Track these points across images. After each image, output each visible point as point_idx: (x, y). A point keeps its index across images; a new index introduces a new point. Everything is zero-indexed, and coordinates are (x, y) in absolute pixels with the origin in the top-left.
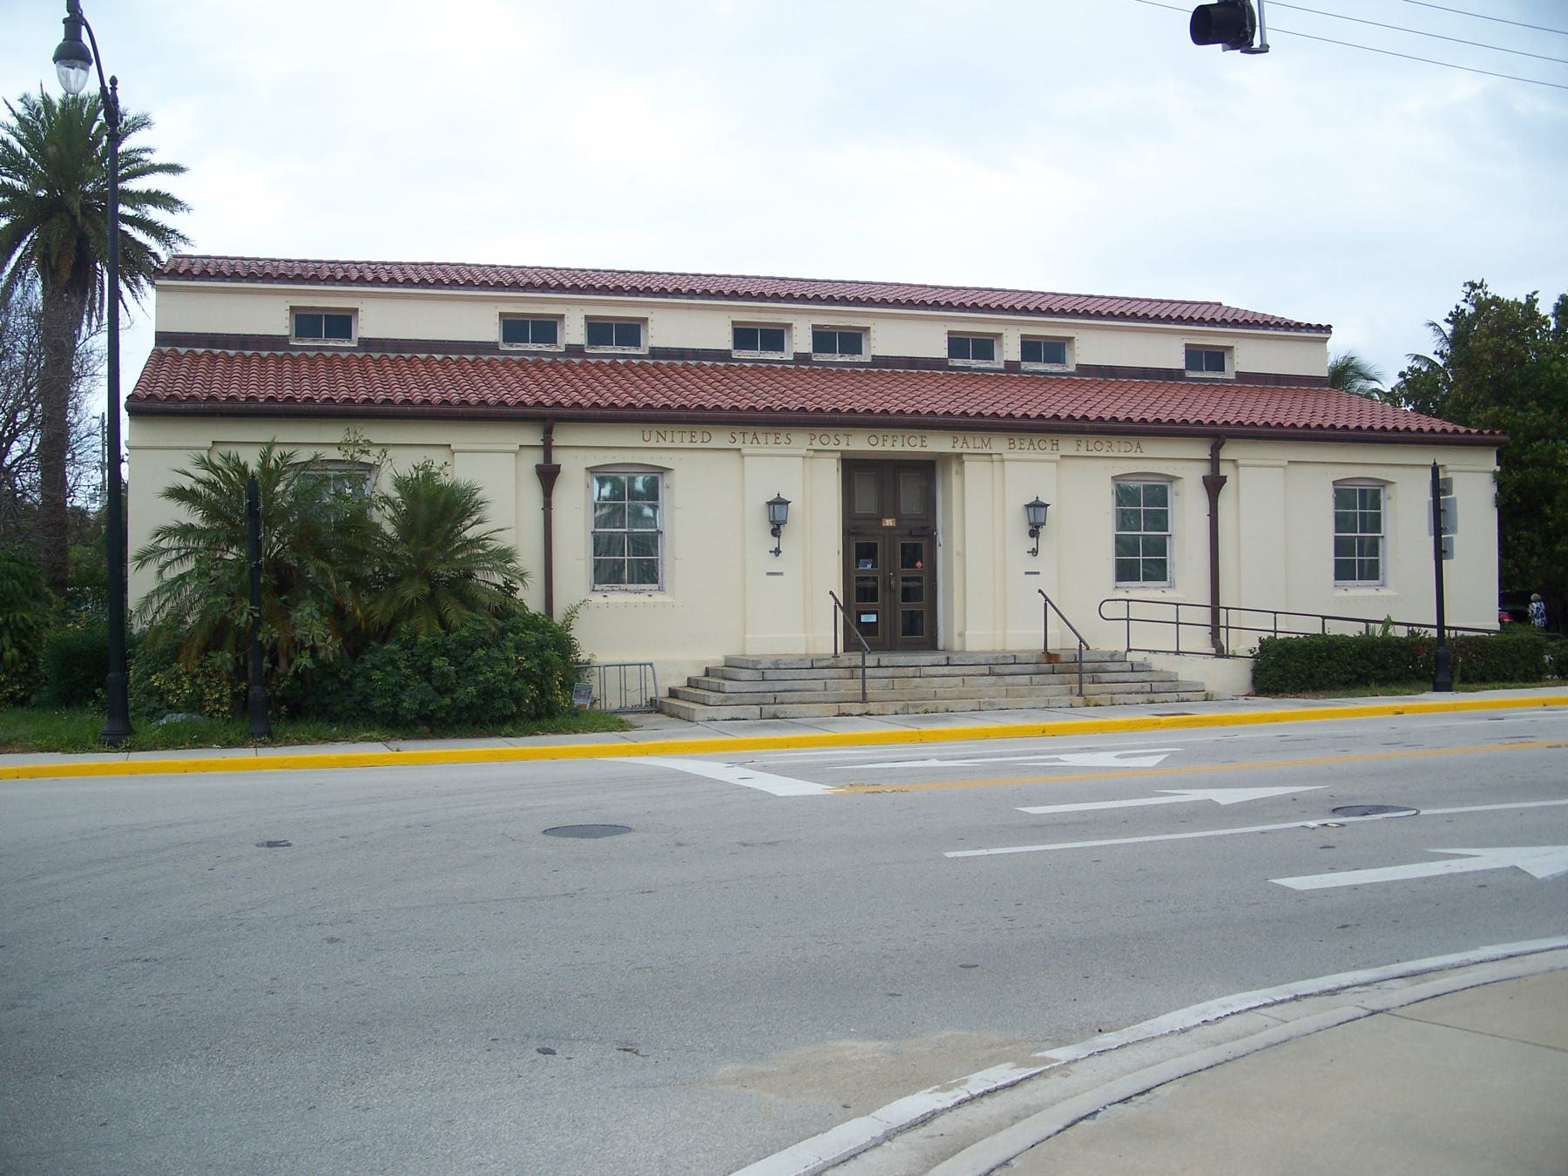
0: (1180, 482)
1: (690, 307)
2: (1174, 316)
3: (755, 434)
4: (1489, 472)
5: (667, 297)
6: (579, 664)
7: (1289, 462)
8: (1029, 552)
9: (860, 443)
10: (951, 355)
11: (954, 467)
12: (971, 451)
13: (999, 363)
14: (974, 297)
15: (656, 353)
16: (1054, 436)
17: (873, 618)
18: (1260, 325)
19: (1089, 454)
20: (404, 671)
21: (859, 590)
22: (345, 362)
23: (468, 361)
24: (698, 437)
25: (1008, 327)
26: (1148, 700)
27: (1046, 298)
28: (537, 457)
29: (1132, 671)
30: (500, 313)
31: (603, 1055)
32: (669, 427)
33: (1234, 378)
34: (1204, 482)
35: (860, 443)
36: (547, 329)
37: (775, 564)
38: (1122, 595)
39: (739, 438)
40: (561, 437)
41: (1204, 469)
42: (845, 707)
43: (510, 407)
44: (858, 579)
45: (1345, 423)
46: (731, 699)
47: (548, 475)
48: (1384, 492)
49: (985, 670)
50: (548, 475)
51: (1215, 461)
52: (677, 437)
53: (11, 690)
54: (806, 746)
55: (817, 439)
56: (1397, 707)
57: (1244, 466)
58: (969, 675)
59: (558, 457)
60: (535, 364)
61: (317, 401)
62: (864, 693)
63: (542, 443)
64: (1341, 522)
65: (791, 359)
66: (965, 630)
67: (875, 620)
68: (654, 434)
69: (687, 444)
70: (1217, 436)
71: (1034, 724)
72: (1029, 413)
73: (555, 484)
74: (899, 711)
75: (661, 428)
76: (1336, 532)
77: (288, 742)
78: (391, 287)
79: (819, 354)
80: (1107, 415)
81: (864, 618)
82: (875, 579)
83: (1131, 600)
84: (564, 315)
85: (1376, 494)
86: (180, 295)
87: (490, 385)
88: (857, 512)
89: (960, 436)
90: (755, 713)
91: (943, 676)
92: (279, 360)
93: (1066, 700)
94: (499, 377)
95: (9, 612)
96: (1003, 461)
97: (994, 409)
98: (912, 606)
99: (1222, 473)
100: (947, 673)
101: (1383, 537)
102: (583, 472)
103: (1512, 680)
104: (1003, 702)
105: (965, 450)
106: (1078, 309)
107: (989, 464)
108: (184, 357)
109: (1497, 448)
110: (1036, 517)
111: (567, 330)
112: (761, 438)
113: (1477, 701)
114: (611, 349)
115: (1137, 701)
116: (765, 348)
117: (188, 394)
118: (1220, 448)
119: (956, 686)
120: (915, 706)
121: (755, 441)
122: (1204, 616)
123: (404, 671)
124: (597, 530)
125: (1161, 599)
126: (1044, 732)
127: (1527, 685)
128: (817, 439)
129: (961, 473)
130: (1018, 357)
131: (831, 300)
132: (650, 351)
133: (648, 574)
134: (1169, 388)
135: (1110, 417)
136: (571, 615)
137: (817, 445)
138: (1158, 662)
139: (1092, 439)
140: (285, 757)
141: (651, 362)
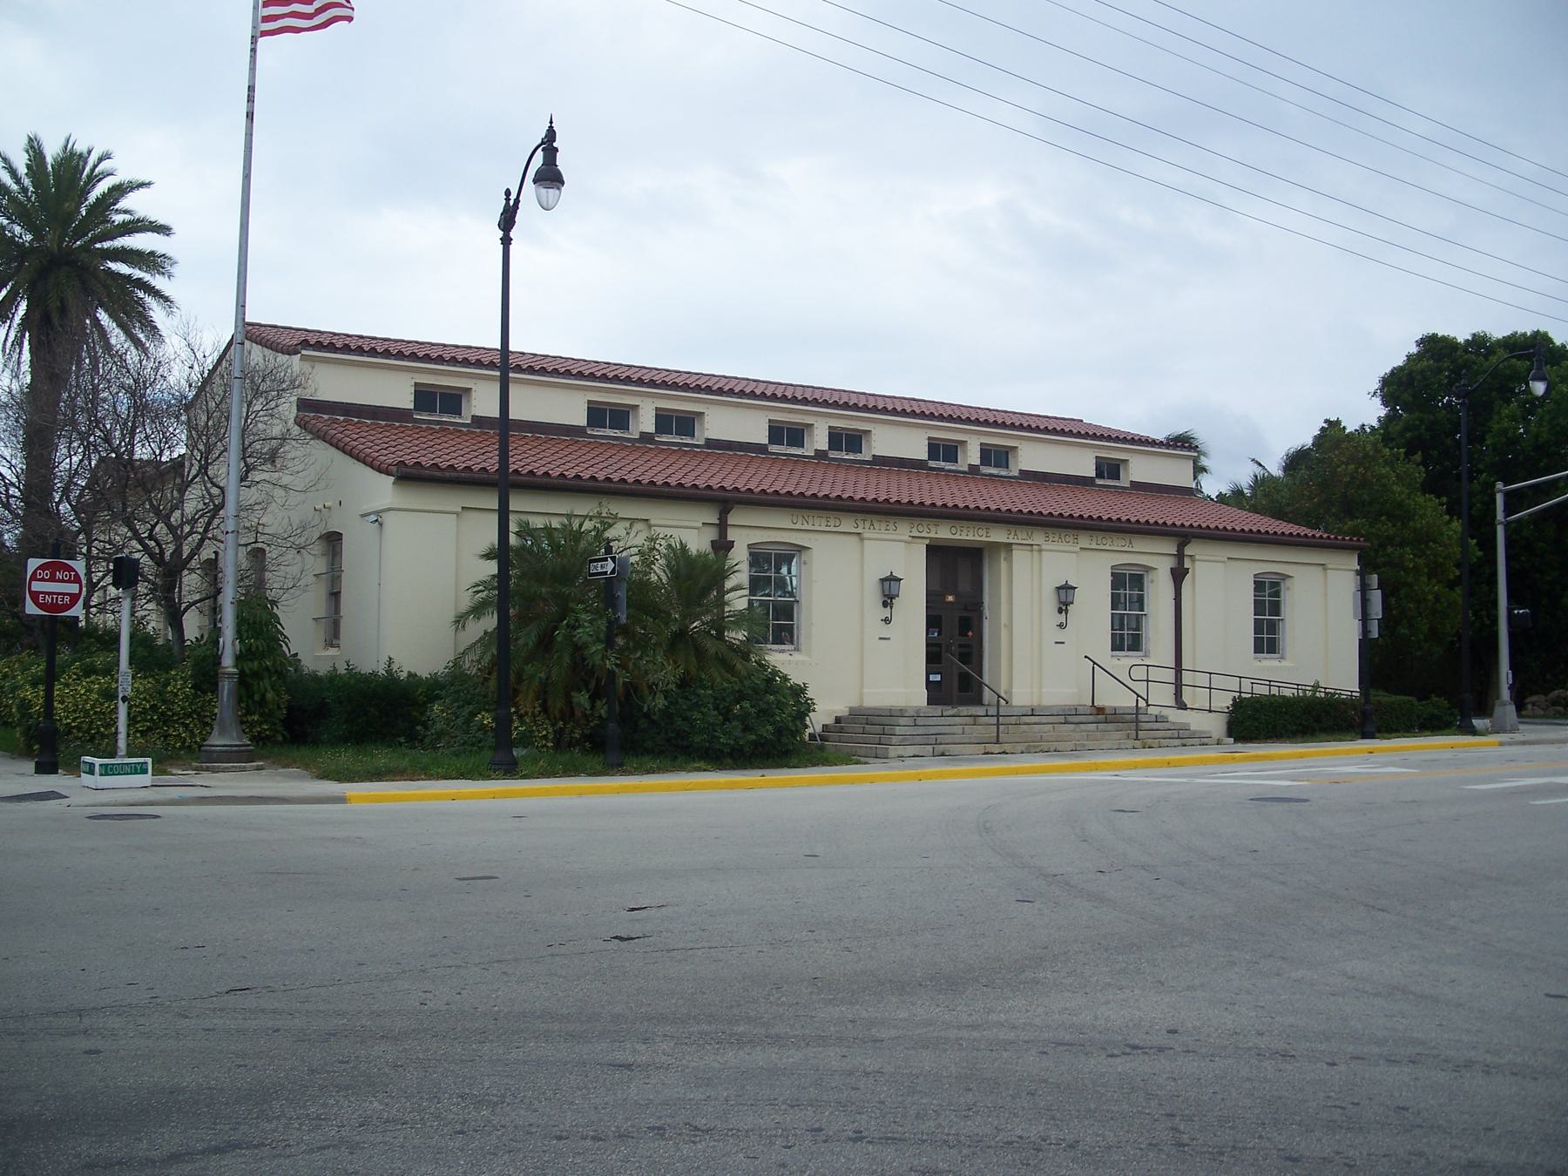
0: (808, 552)
2: (726, 388)
5: (722, 396)
7: (1228, 558)
9: (944, 532)
10: (771, 442)
11: (1003, 555)
12: (1017, 542)
13: (961, 466)
14: (530, 361)
17: (938, 678)
18: (936, 417)
19: (828, 529)
27: (589, 366)
31: (1132, 991)
33: (966, 469)
34: (1172, 574)
35: (944, 532)
37: (885, 631)
39: (860, 524)
45: (875, 496)
46: (907, 740)
48: (1148, 577)
49: (1062, 719)
51: (1180, 556)
52: (817, 521)
53: (259, 729)
54: (1042, 772)
57: (1198, 560)
59: (732, 535)
63: (718, 522)
64: (1116, 602)
66: (1012, 688)
67: (939, 679)
68: (800, 518)
70: (1183, 536)
72: (581, 474)
75: (806, 513)
76: (1255, 615)
80: (616, 477)
85: (1277, 584)
86: (915, 430)
93: (1130, 743)
96: (1040, 551)
99: (730, 538)
100: (1037, 721)
103: (1397, 731)
104: (1090, 744)
105: (1013, 541)
106: (678, 381)
107: (1029, 553)
110: (1065, 596)
113: (1410, 745)
116: (443, 411)
118: (729, 512)
120: (1035, 747)
122: (1170, 675)
127: (1408, 735)
129: (1009, 559)
130: (977, 462)
131: (836, 405)
134: (695, 456)
135: (589, 476)
140: (688, 781)
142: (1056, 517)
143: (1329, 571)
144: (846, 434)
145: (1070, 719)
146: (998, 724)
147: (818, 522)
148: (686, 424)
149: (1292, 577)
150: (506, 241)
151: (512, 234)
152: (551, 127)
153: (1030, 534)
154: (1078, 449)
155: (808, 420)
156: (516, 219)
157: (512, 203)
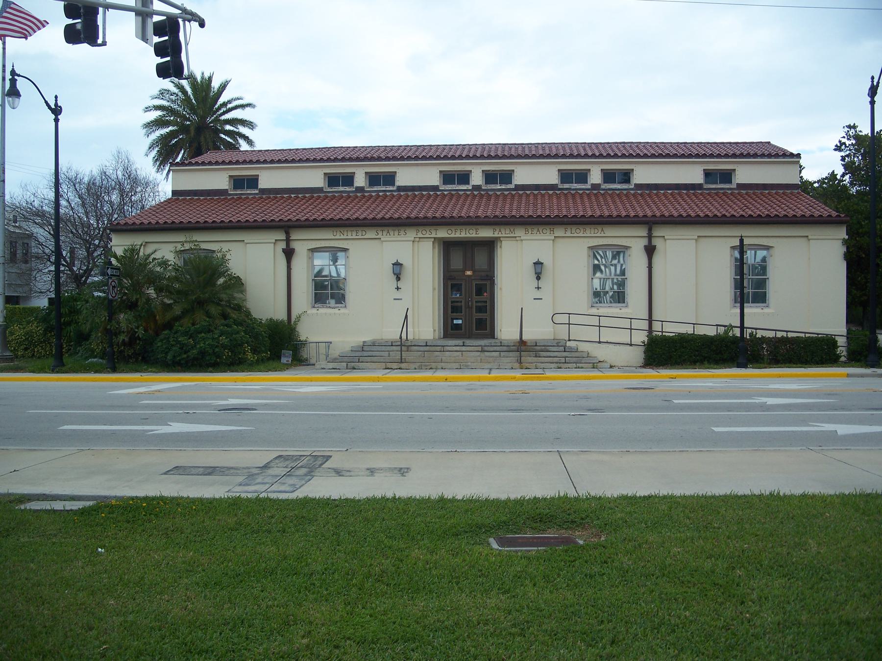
1: (417, 165)
3: (602, 229)
4: (841, 239)
6: (301, 341)
8: (400, 288)
9: (443, 233)
15: (741, 186)
16: (551, 227)
20: (171, 342)
21: (452, 307)
22: (588, 195)
23: (609, 194)
24: (360, 233)
25: (593, 165)
26: (558, 366)
28: (283, 245)
29: (565, 351)
30: (601, 169)
32: (345, 229)
34: (283, 252)
36: (348, 179)
37: (538, 294)
38: (594, 311)
39: (380, 233)
40: (658, 232)
41: (645, 242)
42: (389, 365)
43: (311, 221)
44: (452, 302)
47: (289, 253)
50: (289, 253)
55: (420, 232)
56: (672, 375)
58: (465, 351)
60: (717, 194)
61: (552, 217)
62: (401, 359)
65: (735, 187)
69: (354, 237)
71: (441, 375)
73: (293, 258)
74: (416, 368)
75: (342, 229)
77: (122, 371)
78: (272, 164)
79: (489, 185)
81: (455, 322)
82: (461, 302)
83: (571, 314)
84: (735, 169)
87: (649, 206)
88: (476, 268)
89: (497, 228)
90: (344, 367)
91: (450, 351)
92: (558, 197)
94: (614, 202)
95: (74, 316)
97: (347, 216)
98: (480, 315)
101: (768, 278)
102: (586, 248)
105: (500, 235)
108: (499, 195)
109: (846, 225)
111: (737, 177)
112: (392, 233)
114: (380, 188)
115: (551, 367)
116: (459, 183)
117: (485, 215)
119: (458, 356)
120: (426, 366)
121: (388, 234)
123: (171, 342)
124: (315, 279)
125: (593, 313)
126: (446, 380)
128: (420, 232)
132: (397, 188)
133: (341, 299)
136: (299, 318)
137: (420, 235)
138: (583, 347)
139: (574, 228)
141: (736, 192)
142: (252, 223)
143: (811, 241)
144: (500, 174)
145: (486, 348)
146: (401, 351)
147: (350, 234)
148: (727, 176)
149: (772, 247)
150: (872, 103)
151: (875, 99)
152: (13, 69)
153: (512, 230)
154: (415, 167)
155: (468, 168)
156: (878, 92)
157: (875, 84)
